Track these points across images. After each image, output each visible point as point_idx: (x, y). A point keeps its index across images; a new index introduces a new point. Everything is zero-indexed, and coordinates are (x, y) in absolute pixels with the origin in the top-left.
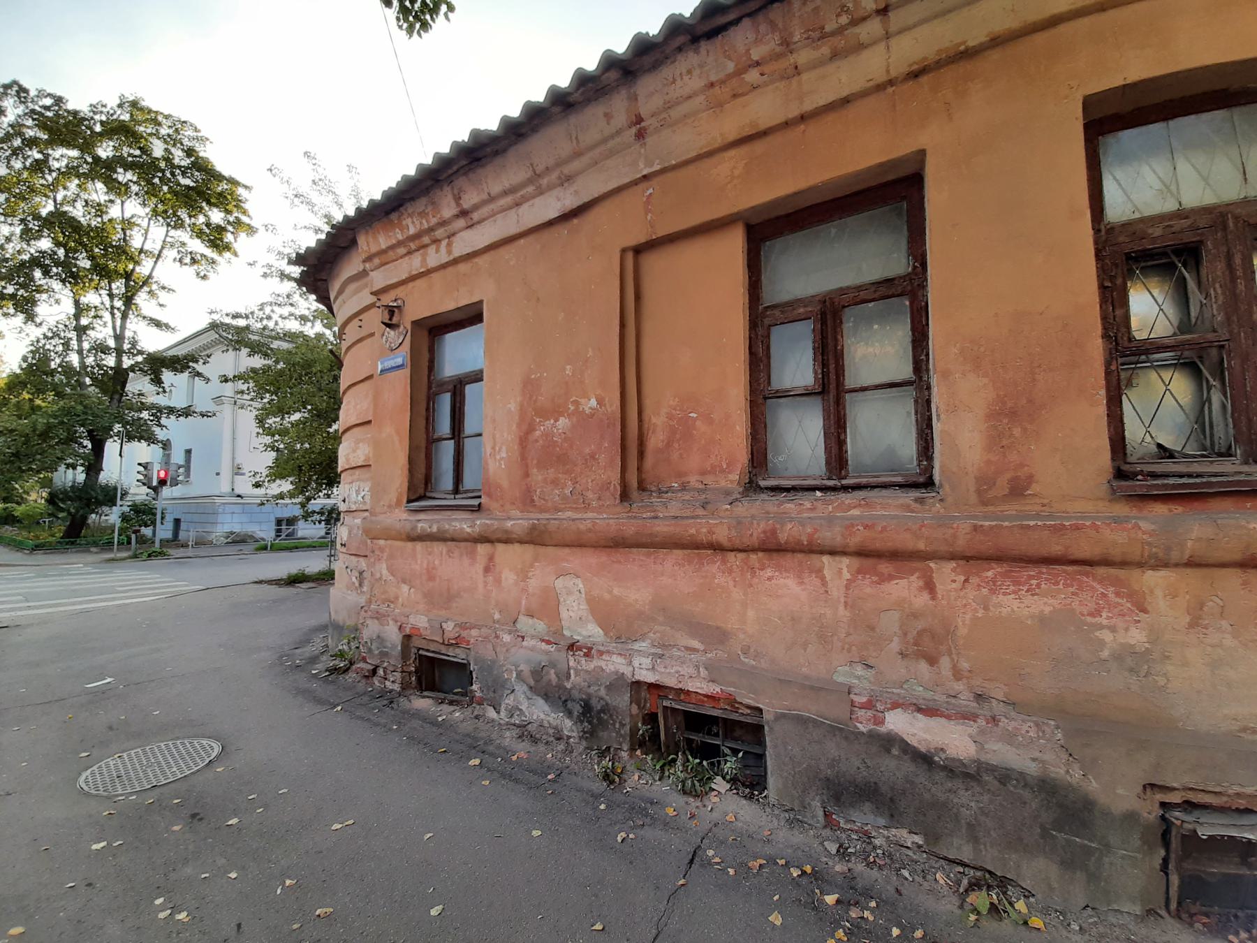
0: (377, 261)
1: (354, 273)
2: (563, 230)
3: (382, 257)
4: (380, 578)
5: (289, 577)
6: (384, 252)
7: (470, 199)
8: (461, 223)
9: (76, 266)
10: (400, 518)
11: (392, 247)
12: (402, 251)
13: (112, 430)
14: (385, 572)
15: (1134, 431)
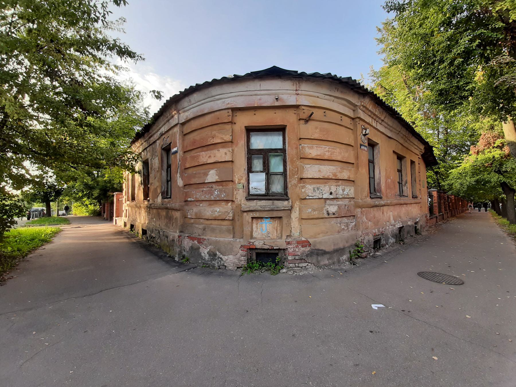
0: (364, 109)
1: (353, 102)
2: (387, 138)
3: (366, 109)
4: (364, 222)
5: (210, 273)
6: (367, 109)
7: (386, 120)
8: (380, 122)
9: (483, 28)
10: (369, 200)
11: (370, 111)
12: (370, 114)
13: (56, 186)
14: (365, 219)
15: (281, 138)
